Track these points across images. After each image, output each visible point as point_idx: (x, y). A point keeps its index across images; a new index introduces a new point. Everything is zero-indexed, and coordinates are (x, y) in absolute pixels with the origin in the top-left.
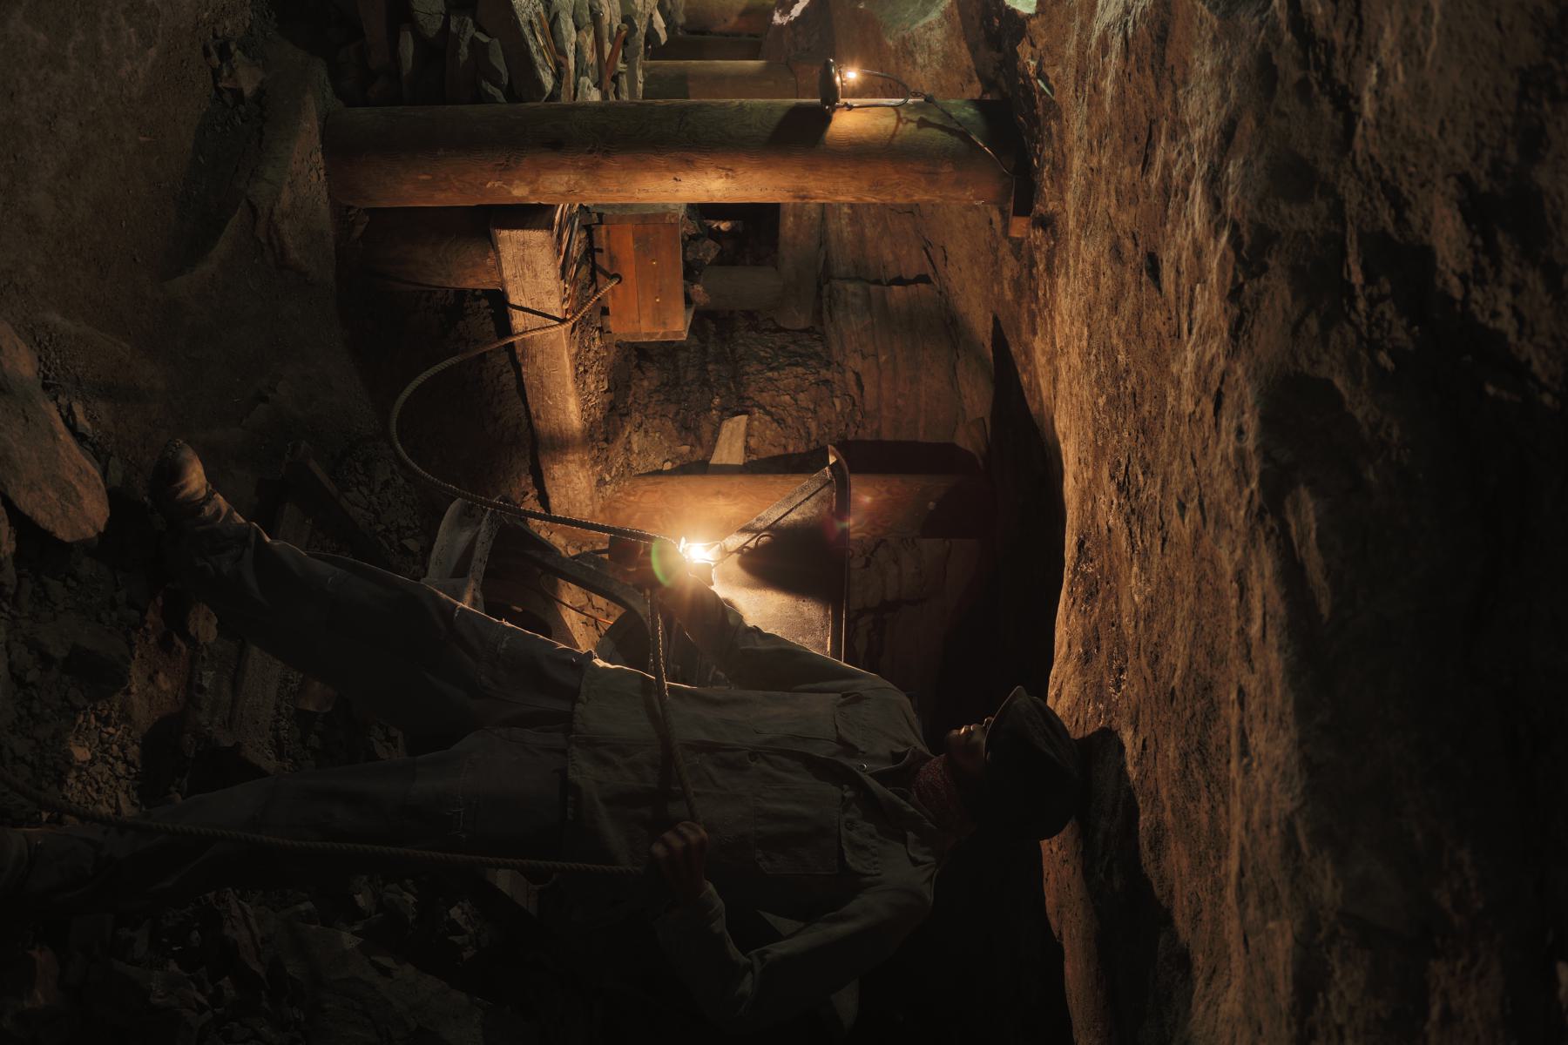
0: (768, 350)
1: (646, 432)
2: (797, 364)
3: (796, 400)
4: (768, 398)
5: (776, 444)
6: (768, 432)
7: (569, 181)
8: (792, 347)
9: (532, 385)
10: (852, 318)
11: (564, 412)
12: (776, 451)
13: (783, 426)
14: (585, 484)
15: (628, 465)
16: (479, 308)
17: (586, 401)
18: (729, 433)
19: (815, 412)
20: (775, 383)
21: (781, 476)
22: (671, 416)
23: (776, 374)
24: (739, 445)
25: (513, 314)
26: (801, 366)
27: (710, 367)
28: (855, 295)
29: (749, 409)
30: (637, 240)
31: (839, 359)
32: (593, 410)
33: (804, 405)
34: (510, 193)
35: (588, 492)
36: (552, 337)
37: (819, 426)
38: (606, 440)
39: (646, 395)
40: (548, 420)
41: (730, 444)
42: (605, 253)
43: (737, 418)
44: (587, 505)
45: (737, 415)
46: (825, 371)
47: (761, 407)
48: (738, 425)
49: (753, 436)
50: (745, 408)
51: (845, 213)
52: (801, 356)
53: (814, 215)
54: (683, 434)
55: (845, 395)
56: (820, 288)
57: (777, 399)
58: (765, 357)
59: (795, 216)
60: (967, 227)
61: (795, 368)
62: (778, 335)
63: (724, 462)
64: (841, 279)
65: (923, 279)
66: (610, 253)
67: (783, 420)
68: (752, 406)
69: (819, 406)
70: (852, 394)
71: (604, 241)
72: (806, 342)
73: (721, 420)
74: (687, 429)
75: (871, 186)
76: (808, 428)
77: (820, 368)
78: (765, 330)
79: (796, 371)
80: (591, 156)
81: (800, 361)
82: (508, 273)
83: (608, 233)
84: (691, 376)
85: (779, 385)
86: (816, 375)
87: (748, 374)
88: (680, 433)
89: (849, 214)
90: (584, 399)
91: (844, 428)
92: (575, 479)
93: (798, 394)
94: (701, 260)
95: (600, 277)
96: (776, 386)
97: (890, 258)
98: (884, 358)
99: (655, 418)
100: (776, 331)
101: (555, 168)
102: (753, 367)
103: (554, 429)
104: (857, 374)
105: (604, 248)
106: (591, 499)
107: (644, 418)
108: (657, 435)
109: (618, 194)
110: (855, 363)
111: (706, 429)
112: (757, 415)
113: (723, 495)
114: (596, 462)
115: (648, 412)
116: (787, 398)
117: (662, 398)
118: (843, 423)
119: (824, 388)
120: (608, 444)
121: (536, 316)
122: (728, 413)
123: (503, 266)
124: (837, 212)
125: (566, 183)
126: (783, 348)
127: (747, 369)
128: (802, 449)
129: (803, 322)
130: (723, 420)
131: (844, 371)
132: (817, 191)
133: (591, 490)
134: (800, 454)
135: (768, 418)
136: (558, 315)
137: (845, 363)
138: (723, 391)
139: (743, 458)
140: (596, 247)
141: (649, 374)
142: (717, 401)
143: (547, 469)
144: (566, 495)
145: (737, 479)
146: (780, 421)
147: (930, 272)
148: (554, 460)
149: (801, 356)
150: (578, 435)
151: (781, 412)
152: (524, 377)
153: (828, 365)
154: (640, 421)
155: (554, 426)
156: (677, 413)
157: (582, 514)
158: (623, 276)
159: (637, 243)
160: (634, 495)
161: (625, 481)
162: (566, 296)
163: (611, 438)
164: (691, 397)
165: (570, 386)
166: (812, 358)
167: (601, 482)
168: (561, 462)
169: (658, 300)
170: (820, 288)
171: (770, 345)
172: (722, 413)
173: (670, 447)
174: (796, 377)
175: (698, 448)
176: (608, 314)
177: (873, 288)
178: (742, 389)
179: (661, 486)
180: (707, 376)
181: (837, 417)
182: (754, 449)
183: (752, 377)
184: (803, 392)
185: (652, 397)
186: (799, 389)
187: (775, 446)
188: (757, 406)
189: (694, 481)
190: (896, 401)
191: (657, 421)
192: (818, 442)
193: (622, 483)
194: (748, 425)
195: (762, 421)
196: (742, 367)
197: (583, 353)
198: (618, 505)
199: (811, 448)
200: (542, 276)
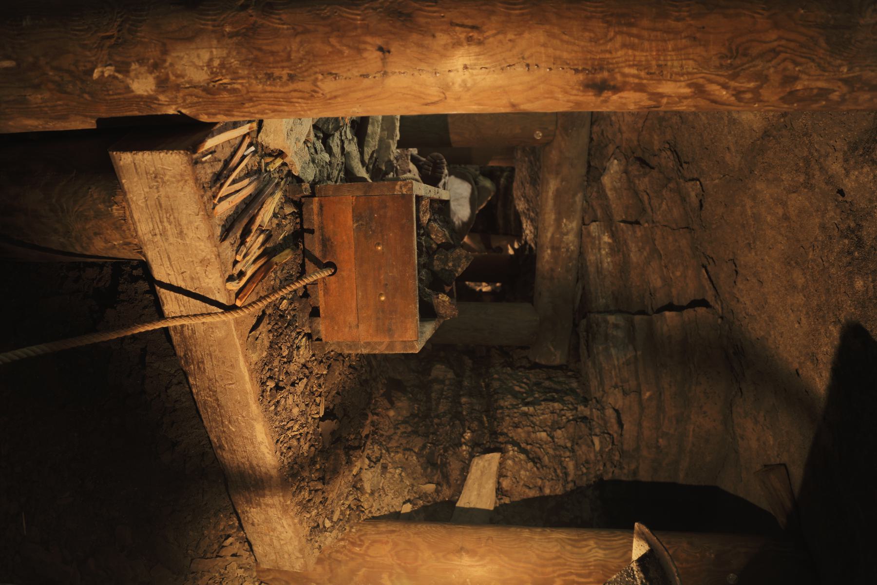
0: (523, 385)
1: (385, 468)
2: (553, 400)
3: (553, 438)
4: (523, 435)
5: (531, 486)
6: (522, 472)
7: (211, 60)
8: (547, 383)
9: (205, 402)
10: (613, 351)
11: (252, 443)
12: (531, 494)
13: (538, 465)
14: (290, 534)
15: (358, 507)
16: (136, 293)
17: (284, 429)
18: (479, 472)
19: (573, 450)
20: (531, 418)
21: (539, 530)
22: (416, 451)
23: (531, 409)
24: (490, 486)
25: (163, 297)
26: (558, 401)
27: (464, 400)
28: (616, 326)
29: (503, 446)
30: (357, 217)
31: (598, 395)
32: (295, 443)
33: (561, 442)
34: (128, 89)
35: (296, 543)
36: (219, 334)
37: (577, 466)
38: (322, 479)
39: (391, 425)
40: (233, 452)
41: (481, 486)
42: (317, 233)
43: (488, 456)
44: (297, 558)
45: (489, 453)
46: (583, 408)
47: (515, 443)
48: (489, 464)
49: (506, 476)
50: (498, 445)
51: (605, 243)
52: (556, 391)
53: (572, 248)
54: (429, 470)
55: (604, 433)
56: (576, 325)
57: (533, 435)
58: (519, 392)
59: (553, 248)
60: (786, 217)
61: (551, 404)
62: (533, 371)
63: (472, 506)
64: (599, 312)
65: (703, 303)
66: (322, 235)
67: (539, 459)
68: (506, 443)
69: (577, 444)
70: (611, 432)
71: (315, 217)
72: (561, 379)
73: (472, 456)
74: (434, 465)
75: (723, 57)
76: (565, 468)
77: (577, 404)
78: (521, 367)
79: (553, 407)
80: (243, 14)
81: (556, 396)
82: (144, 228)
83: (321, 207)
84: (442, 408)
85: (535, 420)
86: (574, 412)
87: (502, 408)
88: (425, 469)
89: (609, 244)
90: (283, 427)
91: (602, 468)
92: (279, 527)
93: (555, 431)
94: (451, 271)
95: (310, 266)
96: (532, 422)
97: (659, 283)
98: (648, 394)
99: (398, 452)
100: (530, 368)
101: (188, 38)
102: (507, 402)
103: (243, 464)
104: (616, 411)
105: (316, 227)
106: (301, 551)
107: (384, 451)
108: (397, 471)
109: (292, 86)
110: (615, 399)
111: (454, 466)
112: (511, 453)
113: (467, 552)
114: (305, 506)
115: (390, 445)
116: (544, 434)
117: (409, 429)
118: (601, 463)
119: (582, 425)
120: (324, 484)
121: (192, 300)
122: (479, 450)
123: (136, 216)
124: (597, 242)
125: (208, 66)
126: (538, 384)
127: (502, 403)
128: (559, 490)
129: (558, 358)
130: (474, 457)
131: (603, 408)
132: (627, 70)
133: (300, 541)
134: (556, 496)
135: (522, 456)
136: (222, 300)
137: (604, 399)
138: (475, 425)
139: (493, 502)
140: (305, 227)
141: (400, 404)
142: (468, 435)
143: (243, 513)
144: (271, 545)
145: (488, 532)
146: (536, 460)
147: (710, 297)
148: (249, 502)
149: (556, 391)
150: (274, 473)
151: (537, 450)
152: (194, 391)
153: (585, 401)
154: (378, 455)
155: (243, 460)
156: (424, 447)
157: (293, 567)
158: (338, 265)
159: (357, 221)
160: (360, 546)
161: (351, 527)
162: (236, 272)
163: (328, 478)
164: (441, 430)
165: (255, 408)
166: (567, 394)
167: (317, 529)
168: (259, 505)
169: (383, 298)
170: (576, 325)
171: (525, 380)
172: (473, 449)
173: (412, 485)
174: (552, 412)
175: (445, 487)
176: (319, 316)
177: (637, 318)
178: (496, 423)
179: (393, 536)
180: (460, 409)
181: (596, 456)
182: (507, 491)
183: (506, 412)
184: (560, 428)
185: (398, 428)
186: (555, 426)
187: (530, 488)
188: (510, 443)
189: (435, 533)
190: (658, 441)
191: (400, 455)
192: (575, 483)
193: (348, 528)
194: (500, 464)
195: (516, 459)
196: (496, 401)
197: (276, 363)
198: (340, 557)
199: (568, 489)
200: (191, 234)
